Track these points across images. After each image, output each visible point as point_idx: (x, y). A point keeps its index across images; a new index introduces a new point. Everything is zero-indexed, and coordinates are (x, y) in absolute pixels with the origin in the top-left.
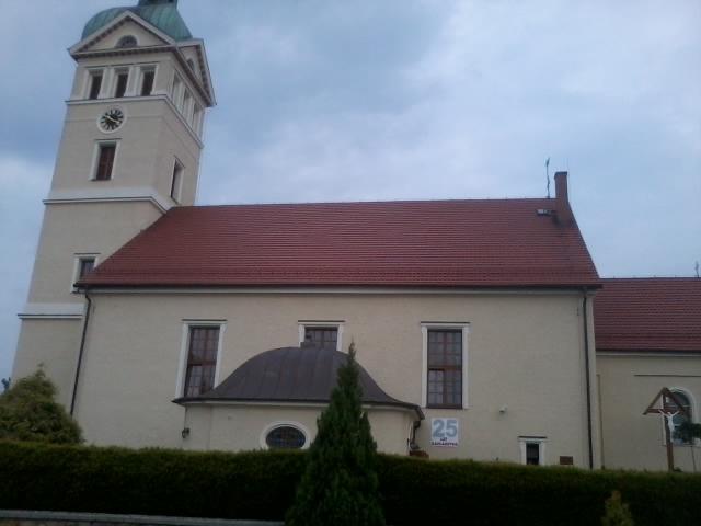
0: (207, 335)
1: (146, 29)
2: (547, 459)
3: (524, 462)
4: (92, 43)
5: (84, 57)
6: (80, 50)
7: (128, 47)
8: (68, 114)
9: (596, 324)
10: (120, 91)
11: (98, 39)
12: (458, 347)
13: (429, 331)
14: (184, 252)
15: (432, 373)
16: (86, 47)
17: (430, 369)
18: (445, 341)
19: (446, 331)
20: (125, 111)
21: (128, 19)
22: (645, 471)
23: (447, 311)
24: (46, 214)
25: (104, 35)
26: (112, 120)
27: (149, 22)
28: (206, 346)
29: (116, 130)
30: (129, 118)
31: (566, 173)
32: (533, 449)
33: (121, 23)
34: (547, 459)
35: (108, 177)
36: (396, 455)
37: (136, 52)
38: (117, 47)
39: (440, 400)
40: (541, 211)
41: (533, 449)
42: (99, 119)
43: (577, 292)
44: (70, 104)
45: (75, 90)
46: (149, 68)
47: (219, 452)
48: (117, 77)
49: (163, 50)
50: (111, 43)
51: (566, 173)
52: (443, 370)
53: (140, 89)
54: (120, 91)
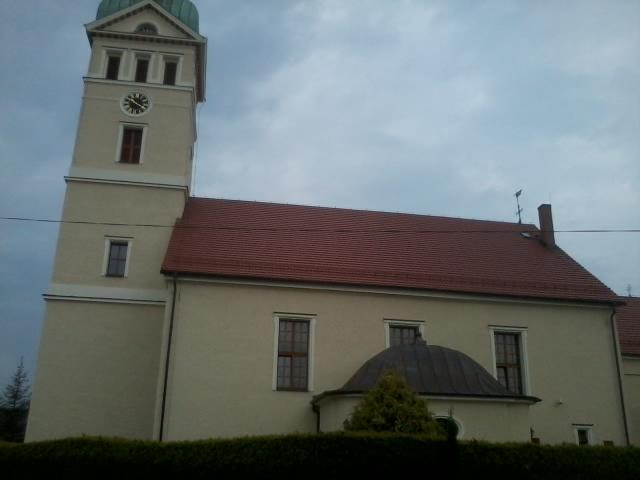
0: (402, 334)
1: (167, 19)
2: (593, 440)
3: (577, 443)
4: (109, 24)
5: (102, 35)
6: (97, 28)
7: (146, 34)
8: (86, 92)
9: (620, 335)
10: (141, 74)
11: (116, 21)
12: (282, 329)
13: (281, 320)
14: (226, 246)
15: (282, 359)
16: (103, 27)
17: (279, 356)
18: (510, 341)
19: (294, 322)
20: (150, 96)
21: (149, 7)
22: (84, 435)
23: (296, 303)
24: (68, 192)
25: (122, 18)
26: (137, 104)
27: (170, 11)
28: (293, 337)
29: (141, 114)
30: (155, 105)
31: (549, 206)
32: (583, 434)
33: (141, 9)
34: (593, 440)
35: (135, 159)
36: (116, 438)
37: (151, 40)
38: (135, 32)
39: (287, 383)
40: (526, 235)
41: (583, 434)
42: (121, 101)
43: (607, 307)
44: (87, 80)
45: (92, 66)
46: (145, 56)
47: (201, 441)
48: (107, 59)
49: (187, 44)
50: (130, 27)
51: (549, 206)
52: (291, 356)
53: (105, 71)
54: (141, 74)
